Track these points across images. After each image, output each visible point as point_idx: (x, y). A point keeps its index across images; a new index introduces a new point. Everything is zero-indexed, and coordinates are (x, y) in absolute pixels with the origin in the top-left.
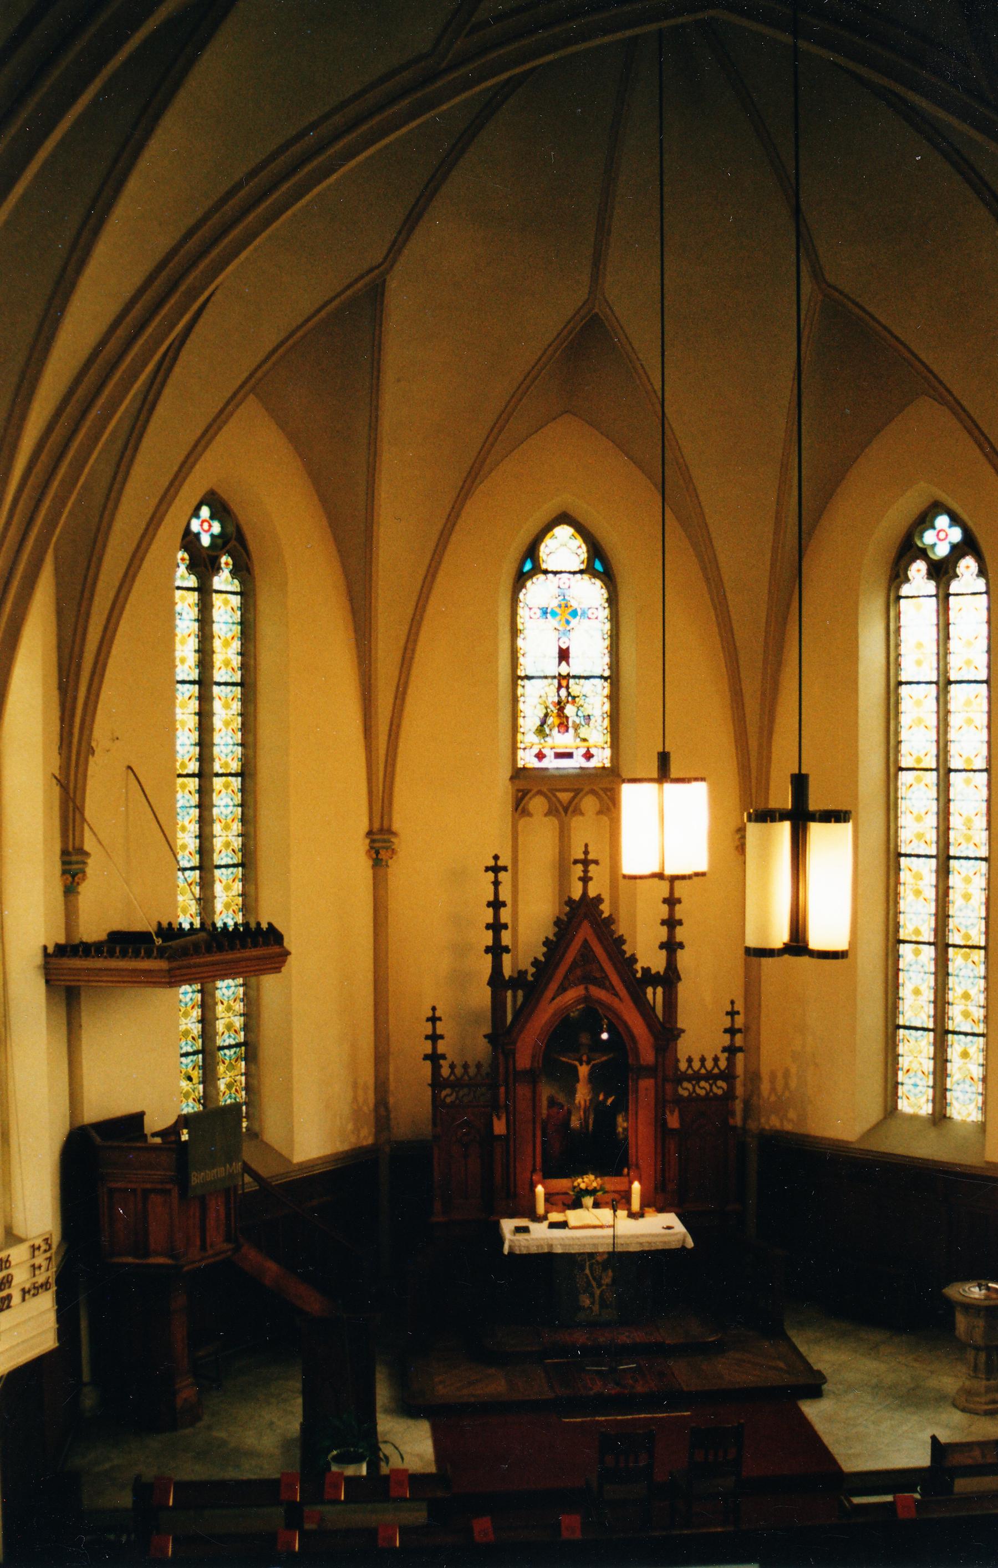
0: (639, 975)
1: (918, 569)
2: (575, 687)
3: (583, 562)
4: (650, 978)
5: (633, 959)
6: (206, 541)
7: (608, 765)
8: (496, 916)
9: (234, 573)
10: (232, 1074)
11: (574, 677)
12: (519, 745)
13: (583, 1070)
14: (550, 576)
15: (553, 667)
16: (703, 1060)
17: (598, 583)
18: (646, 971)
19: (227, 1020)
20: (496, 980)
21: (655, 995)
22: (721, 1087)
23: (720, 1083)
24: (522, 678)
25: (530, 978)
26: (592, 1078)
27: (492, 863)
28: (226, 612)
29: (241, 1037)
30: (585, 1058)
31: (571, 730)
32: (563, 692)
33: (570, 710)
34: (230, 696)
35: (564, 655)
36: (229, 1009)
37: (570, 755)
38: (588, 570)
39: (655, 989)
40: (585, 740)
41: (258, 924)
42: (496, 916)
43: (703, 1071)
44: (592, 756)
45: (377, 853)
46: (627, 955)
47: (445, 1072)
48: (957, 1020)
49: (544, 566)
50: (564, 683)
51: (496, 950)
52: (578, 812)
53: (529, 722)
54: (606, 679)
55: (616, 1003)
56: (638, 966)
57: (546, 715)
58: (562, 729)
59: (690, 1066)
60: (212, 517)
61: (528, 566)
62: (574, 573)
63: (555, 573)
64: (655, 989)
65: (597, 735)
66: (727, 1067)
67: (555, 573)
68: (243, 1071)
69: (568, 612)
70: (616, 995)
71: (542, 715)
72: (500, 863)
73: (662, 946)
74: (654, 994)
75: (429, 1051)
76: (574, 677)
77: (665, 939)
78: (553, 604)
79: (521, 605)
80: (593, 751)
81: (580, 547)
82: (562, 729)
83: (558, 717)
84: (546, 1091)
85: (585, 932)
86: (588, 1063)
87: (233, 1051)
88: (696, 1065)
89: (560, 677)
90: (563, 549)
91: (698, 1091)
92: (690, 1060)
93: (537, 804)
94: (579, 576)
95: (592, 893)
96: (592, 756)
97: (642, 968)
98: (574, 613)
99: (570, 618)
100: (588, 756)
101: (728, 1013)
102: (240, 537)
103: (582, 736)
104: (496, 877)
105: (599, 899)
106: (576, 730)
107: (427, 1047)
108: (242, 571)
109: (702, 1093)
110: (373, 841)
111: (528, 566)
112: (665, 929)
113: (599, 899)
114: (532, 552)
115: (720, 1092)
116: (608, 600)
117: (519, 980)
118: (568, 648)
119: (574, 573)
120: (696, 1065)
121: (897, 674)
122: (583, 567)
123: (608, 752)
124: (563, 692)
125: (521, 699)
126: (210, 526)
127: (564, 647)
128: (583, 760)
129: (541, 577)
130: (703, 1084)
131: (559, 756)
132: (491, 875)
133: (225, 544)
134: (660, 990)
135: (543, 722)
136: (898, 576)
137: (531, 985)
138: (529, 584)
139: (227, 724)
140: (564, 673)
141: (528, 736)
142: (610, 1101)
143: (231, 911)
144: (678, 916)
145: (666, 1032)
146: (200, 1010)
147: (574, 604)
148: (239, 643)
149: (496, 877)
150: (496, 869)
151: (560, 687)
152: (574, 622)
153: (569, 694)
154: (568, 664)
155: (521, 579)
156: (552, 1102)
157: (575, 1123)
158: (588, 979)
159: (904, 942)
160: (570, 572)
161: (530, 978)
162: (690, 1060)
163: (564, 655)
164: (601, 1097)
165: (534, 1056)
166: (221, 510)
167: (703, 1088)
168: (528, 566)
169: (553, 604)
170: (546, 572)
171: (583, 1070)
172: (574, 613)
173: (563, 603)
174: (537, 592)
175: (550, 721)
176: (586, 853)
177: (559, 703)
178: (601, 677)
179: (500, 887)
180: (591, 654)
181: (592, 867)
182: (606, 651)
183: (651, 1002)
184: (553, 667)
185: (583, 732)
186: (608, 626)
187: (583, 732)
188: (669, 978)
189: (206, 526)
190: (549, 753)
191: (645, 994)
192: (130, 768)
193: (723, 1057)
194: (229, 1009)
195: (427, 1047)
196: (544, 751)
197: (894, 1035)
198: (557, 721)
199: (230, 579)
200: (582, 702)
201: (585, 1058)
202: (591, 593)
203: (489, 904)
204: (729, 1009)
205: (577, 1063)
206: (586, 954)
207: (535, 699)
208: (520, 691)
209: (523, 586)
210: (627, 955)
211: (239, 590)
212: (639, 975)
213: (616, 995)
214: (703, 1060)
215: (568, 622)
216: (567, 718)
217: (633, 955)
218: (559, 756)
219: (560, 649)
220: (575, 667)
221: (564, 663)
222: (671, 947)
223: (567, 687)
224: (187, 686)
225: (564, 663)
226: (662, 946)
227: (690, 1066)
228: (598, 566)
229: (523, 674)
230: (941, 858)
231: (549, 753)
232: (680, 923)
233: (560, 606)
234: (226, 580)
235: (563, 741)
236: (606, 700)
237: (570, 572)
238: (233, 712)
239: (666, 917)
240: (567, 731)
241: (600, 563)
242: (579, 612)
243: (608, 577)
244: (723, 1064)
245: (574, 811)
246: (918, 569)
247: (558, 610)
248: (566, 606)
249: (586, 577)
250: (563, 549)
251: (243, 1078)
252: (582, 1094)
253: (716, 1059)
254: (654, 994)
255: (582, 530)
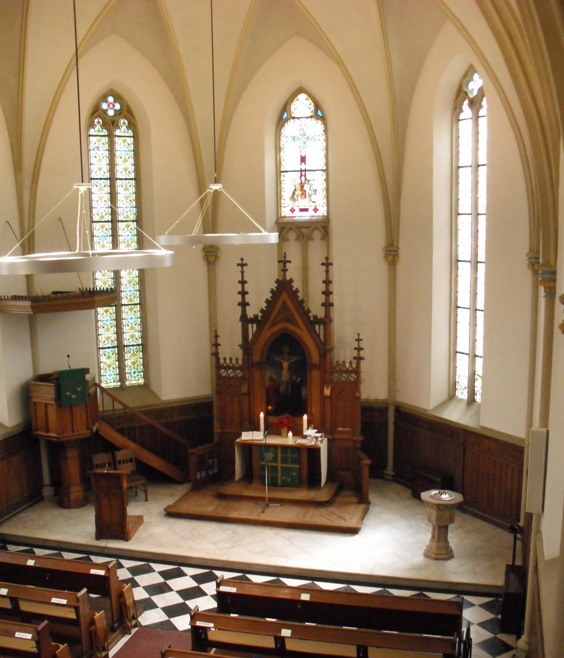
0: (312, 319)
1: (465, 105)
2: (309, 175)
3: (312, 112)
4: (317, 321)
5: (309, 311)
6: (111, 113)
7: (326, 214)
8: (243, 288)
9: (129, 127)
10: (135, 358)
11: (308, 170)
12: (282, 205)
13: (286, 364)
14: (296, 120)
15: (298, 166)
16: (231, 359)
17: (320, 122)
18: (315, 317)
19: (131, 334)
20: (245, 320)
21: (319, 329)
22: (353, 377)
23: (353, 375)
24: (283, 172)
25: (260, 319)
26: (290, 367)
27: (240, 262)
28: (124, 146)
29: (140, 342)
30: (286, 358)
31: (307, 197)
32: (303, 178)
33: (306, 187)
34: (128, 185)
35: (303, 159)
36: (132, 328)
37: (306, 210)
38: (315, 116)
39: (252, 325)
40: (314, 202)
41: (90, 288)
42: (243, 288)
43: (237, 365)
44: (318, 210)
45: (207, 258)
46: (294, 289)
47: (222, 361)
48: (127, 339)
49: (293, 115)
50: (303, 173)
51: (244, 304)
52: (312, 239)
53: (286, 194)
54: (324, 171)
55: (298, 331)
56: (311, 314)
57: (295, 190)
58: (303, 197)
59: (225, 362)
60: (115, 101)
61: (285, 116)
62: (308, 118)
63: (298, 118)
64: (252, 325)
65: (320, 200)
66: (357, 367)
67: (298, 118)
68: (141, 357)
69: (305, 137)
70: (300, 328)
71: (293, 190)
72: (244, 262)
73: (239, 304)
74: (319, 328)
75: (356, 355)
76: (308, 170)
77: (324, 301)
78: (298, 134)
79: (282, 135)
80: (318, 207)
81: (310, 104)
82: (303, 197)
83: (302, 190)
84: (269, 373)
85: (284, 296)
86: (288, 360)
87: (135, 347)
88: (228, 362)
89: (301, 171)
90: (302, 106)
91: (351, 378)
92: (225, 359)
93: (292, 235)
94: (310, 119)
95: (288, 278)
96: (318, 210)
97: (313, 316)
98: (308, 138)
99: (306, 141)
100: (316, 210)
101: (356, 340)
102: (129, 111)
103: (313, 200)
104: (242, 269)
105: (291, 281)
106: (310, 197)
107: (355, 353)
108: (132, 126)
109: (344, 379)
110: (206, 252)
111: (283, 116)
112: (240, 296)
113: (291, 281)
114: (286, 108)
115: (353, 379)
116: (324, 131)
117: (255, 320)
118: (305, 156)
119: (308, 118)
120: (228, 362)
121: (280, 168)
122: (312, 114)
123: (325, 208)
124: (303, 178)
125: (283, 182)
126: (114, 106)
127: (303, 155)
128: (313, 212)
129: (292, 120)
130: (344, 375)
131: (302, 210)
132: (240, 268)
133: (120, 114)
134: (322, 326)
135: (294, 194)
136: (457, 109)
137: (261, 321)
138: (286, 124)
139: (126, 198)
140: (303, 169)
141: (286, 202)
142: (298, 380)
143: (132, 284)
144: (246, 290)
145: (325, 348)
146: (115, 329)
147: (308, 134)
148: (133, 160)
149: (242, 269)
150: (242, 265)
151: (301, 175)
152: (308, 143)
153: (306, 179)
154: (305, 164)
155: (281, 122)
156: (271, 379)
157: (282, 389)
158: (287, 320)
159: (459, 307)
160: (306, 118)
161: (260, 319)
162: (225, 359)
163: (303, 159)
164: (294, 378)
165: (261, 356)
166: (118, 98)
167: (231, 373)
168: (320, 113)
169: (298, 134)
170: (294, 118)
171: (286, 364)
172: (308, 138)
173: (303, 133)
174: (290, 129)
175: (297, 193)
176: (285, 257)
177: (301, 184)
178: (322, 170)
179: (244, 274)
180: (317, 160)
181: (288, 264)
182: (324, 157)
183: (318, 332)
184: (298, 166)
185: (314, 198)
186: (325, 144)
187: (314, 198)
188: (326, 321)
189: (111, 106)
190: (297, 210)
191: (315, 328)
192: (60, 218)
193: (354, 362)
194: (132, 328)
195: (355, 353)
196: (294, 208)
197: (455, 357)
198: (300, 193)
199: (101, 129)
200: (312, 183)
201: (286, 358)
202: (317, 127)
203: (239, 282)
204: (357, 338)
205: (282, 361)
206: (285, 307)
207: (290, 182)
208: (282, 178)
209: (283, 126)
210: (294, 289)
211: (132, 135)
212: (312, 319)
213: (300, 328)
214: (231, 359)
215: (305, 143)
216: (305, 191)
217: (309, 309)
218: (302, 210)
219: (301, 156)
220: (309, 165)
221: (303, 163)
222: (328, 305)
223: (305, 176)
224: (103, 181)
225: (303, 163)
226: (239, 304)
227: (225, 362)
228: (320, 113)
229: (283, 170)
230: (472, 262)
231: (297, 210)
232: (247, 293)
233: (301, 135)
234: (124, 130)
235: (303, 203)
236: (324, 182)
237: (306, 118)
238: (105, 192)
239: (324, 290)
240: (305, 198)
241: (319, 112)
242: (310, 137)
243: (323, 119)
244: (354, 365)
245: (299, 237)
246: (465, 105)
247: (300, 137)
248: (304, 135)
249: (313, 119)
250: (302, 106)
251: (141, 360)
252: (285, 375)
253: (351, 363)
254: (319, 328)
255: (311, 96)
